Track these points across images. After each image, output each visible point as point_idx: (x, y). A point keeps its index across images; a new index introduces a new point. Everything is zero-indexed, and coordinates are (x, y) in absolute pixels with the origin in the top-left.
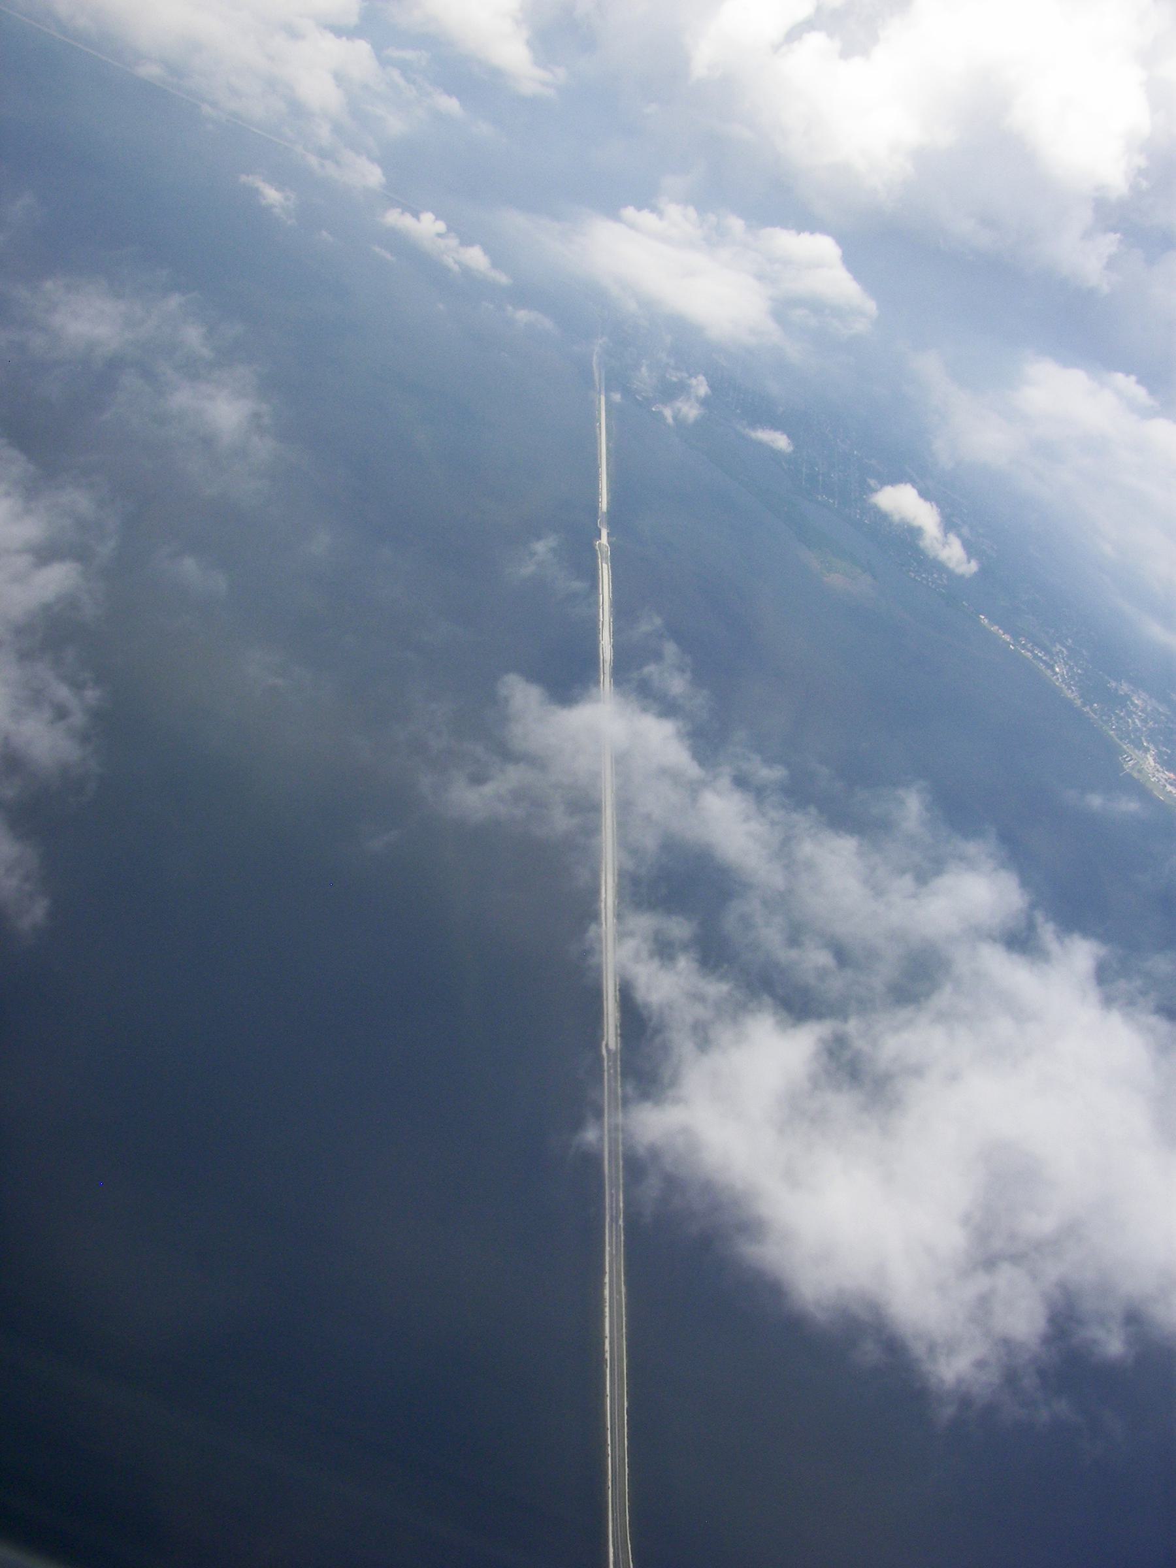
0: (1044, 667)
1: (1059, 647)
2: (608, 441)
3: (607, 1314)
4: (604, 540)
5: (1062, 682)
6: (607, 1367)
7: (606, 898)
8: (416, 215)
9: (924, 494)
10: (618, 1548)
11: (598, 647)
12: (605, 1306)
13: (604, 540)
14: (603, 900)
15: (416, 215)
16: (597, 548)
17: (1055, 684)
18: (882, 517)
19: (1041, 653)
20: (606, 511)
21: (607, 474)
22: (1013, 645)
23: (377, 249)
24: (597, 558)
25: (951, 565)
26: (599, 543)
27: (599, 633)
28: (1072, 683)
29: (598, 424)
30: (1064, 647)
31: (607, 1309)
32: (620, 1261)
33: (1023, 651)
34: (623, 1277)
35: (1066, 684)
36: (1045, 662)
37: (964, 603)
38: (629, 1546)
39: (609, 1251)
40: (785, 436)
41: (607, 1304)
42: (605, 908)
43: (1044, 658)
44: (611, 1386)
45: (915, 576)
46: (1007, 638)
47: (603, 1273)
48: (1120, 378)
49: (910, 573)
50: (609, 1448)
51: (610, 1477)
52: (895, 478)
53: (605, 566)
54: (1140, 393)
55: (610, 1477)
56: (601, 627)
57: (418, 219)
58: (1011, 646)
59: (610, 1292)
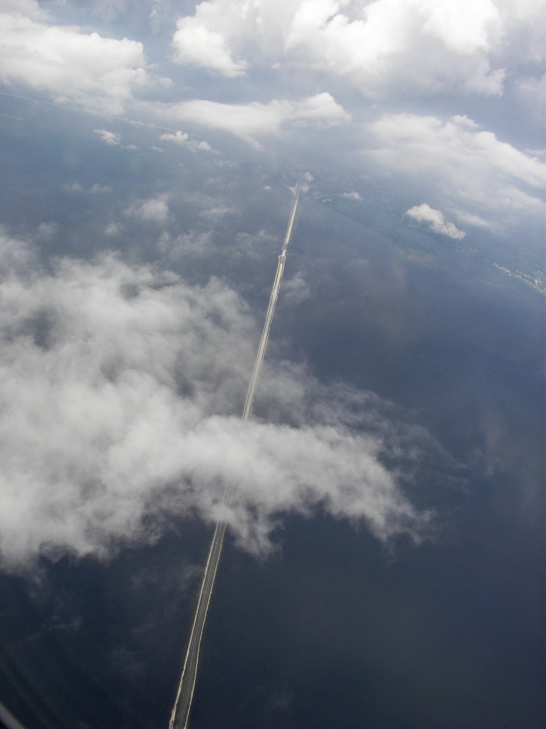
0: (528, 281)
1: (539, 272)
2: (295, 216)
3: (210, 557)
4: (284, 254)
5: (538, 286)
6: (204, 578)
7: (250, 393)
8: (174, 133)
9: (432, 207)
10: (192, 652)
11: (270, 296)
12: (210, 553)
13: (284, 254)
14: (248, 393)
15: (174, 133)
16: (279, 258)
17: (533, 288)
18: (414, 221)
19: (527, 275)
20: (287, 243)
21: (292, 229)
22: (510, 274)
23: (155, 148)
24: (278, 262)
25: (451, 235)
26: (281, 256)
27: (272, 291)
28: (544, 286)
29: (291, 211)
30: (542, 272)
31: (210, 555)
32: (222, 534)
33: (517, 276)
34: (222, 541)
35: (540, 287)
36: (529, 279)
37: (485, 259)
38: (199, 651)
39: (217, 531)
40: (356, 193)
41: (211, 552)
42: (249, 396)
43: (529, 277)
44: (204, 586)
45: (458, 251)
46: (508, 271)
47: (212, 539)
48: (458, 118)
49: (456, 251)
50: (197, 611)
51: (195, 622)
52: (418, 204)
53: (281, 265)
54: (471, 123)
55: (195, 622)
56: (273, 288)
57: (176, 135)
58: (510, 274)
59: (213, 548)
